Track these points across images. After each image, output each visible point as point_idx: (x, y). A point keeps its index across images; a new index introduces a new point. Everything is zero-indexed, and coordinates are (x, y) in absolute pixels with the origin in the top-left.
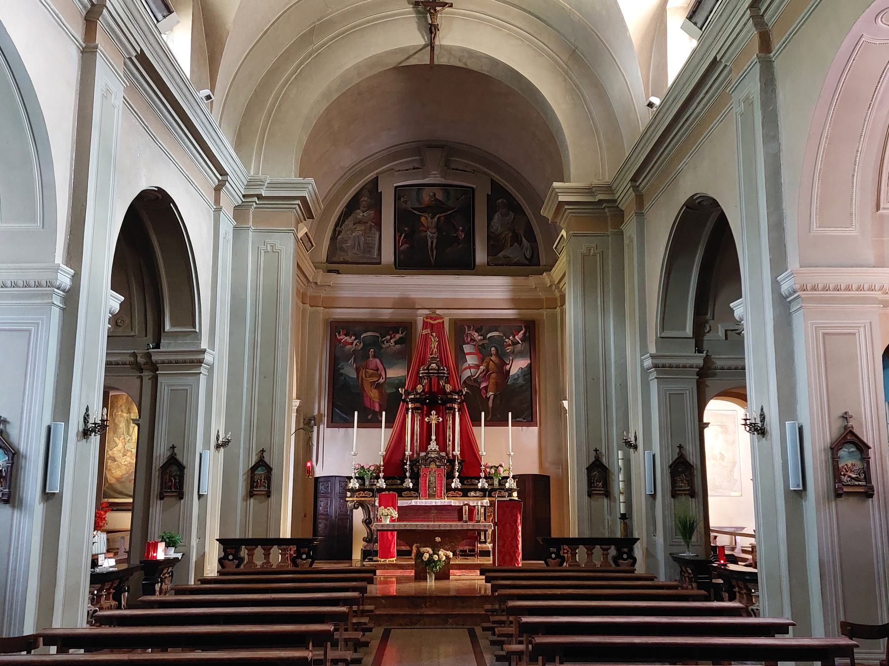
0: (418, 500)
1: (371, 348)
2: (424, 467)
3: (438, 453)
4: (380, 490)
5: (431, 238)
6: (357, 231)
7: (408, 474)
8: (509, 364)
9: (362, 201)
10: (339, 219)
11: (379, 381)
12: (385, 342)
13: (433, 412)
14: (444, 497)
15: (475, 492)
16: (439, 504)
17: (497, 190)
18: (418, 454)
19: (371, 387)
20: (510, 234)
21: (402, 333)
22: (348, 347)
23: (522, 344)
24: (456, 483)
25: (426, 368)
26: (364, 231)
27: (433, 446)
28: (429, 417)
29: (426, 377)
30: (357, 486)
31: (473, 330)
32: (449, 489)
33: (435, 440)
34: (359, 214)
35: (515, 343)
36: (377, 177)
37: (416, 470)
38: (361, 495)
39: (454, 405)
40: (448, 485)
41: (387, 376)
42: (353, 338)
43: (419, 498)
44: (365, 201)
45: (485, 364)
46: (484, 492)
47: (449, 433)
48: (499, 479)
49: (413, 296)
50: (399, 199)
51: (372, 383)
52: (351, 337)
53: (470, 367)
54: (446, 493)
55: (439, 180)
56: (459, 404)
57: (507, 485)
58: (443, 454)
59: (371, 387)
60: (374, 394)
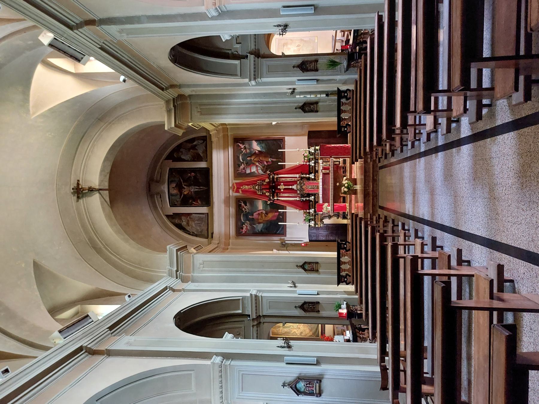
0: (320, 193)
3: (298, 185)
4: (315, 211)
7: (308, 199)
10: (187, 233)
13: (279, 187)
16: (322, 184)
18: (298, 194)
22: (248, 228)
24: (312, 176)
25: (258, 191)
27: (294, 187)
30: (313, 222)
35: (245, 148)
37: (306, 195)
40: (313, 180)
42: (244, 225)
45: (255, 163)
46: (316, 162)
47: (288, 180)
50: (176, 205)
53: (257, 170)
57: (313, 151)
58: (298, 182)
60: (270, 215)
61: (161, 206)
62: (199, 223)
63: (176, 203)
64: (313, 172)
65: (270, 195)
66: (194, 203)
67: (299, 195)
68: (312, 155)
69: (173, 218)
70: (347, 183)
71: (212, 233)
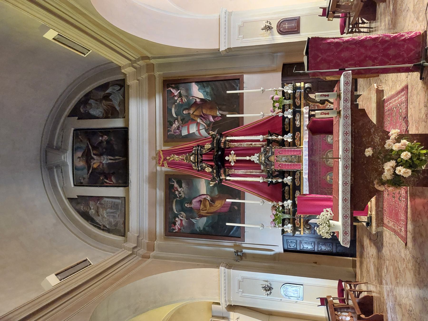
0: (304, 171)
1: (185, 205)
2: (273, 166)
3: (261, 154)
4: (294, 205)
5: (107, 160)
6: (103, 214)
7: (280, 180)
8: (196, 99)
9: (84, 210)
10: (95, 226)
11: (209, 200)
12: (180, 195)
13: (227, 158)
14: (300, 148)
15: (296, 120)
16: (307, 153)
17: (74, 113)
18: (263, 171)
19: (213, 206)
20: (104, 101)
21: (174, 182)
22: (184, 223)
23: (181, 90)
24: (288, 138)
25: (193, 165)
26: (103, 209)
27: (255, 158)
28: (231, 162)
29: (201, 164)
30: (290, 225)
31: (171, 128)
32: (293, 144)
33: (250, 157)
34: (92, 212)
35: (180, 95)
36: (68, 198)
37: (276, 173)
38: (299, 222)
39: (222, 141)
40: (289, 144)
41: (206, 194)
42: (177, 219)
43: (301, 171)
44: (83, 208)
45: (196, 118)
46: (297, 112)
47: (245, 144)
48: (284, 99)
49: (148, 174)
50: (81, 183)
51: (211, 205)
52: (177, 221)
53: (199, 130)
54: (297, 146)
55: (69, 152)
56: (222, 137)
57: (290, 91)
58: (262, 149)
59: (213, 206)
60: (218, 204)
61: (63, 184)
62: (112, 213)
63: (82, 181)
64: (291, 130)
65: (213, 172)
66: (107, 181)
67: (264, 173)
68: (289, 99)
69: (78, 203)
70: (409, 149)
71: (129, 229)
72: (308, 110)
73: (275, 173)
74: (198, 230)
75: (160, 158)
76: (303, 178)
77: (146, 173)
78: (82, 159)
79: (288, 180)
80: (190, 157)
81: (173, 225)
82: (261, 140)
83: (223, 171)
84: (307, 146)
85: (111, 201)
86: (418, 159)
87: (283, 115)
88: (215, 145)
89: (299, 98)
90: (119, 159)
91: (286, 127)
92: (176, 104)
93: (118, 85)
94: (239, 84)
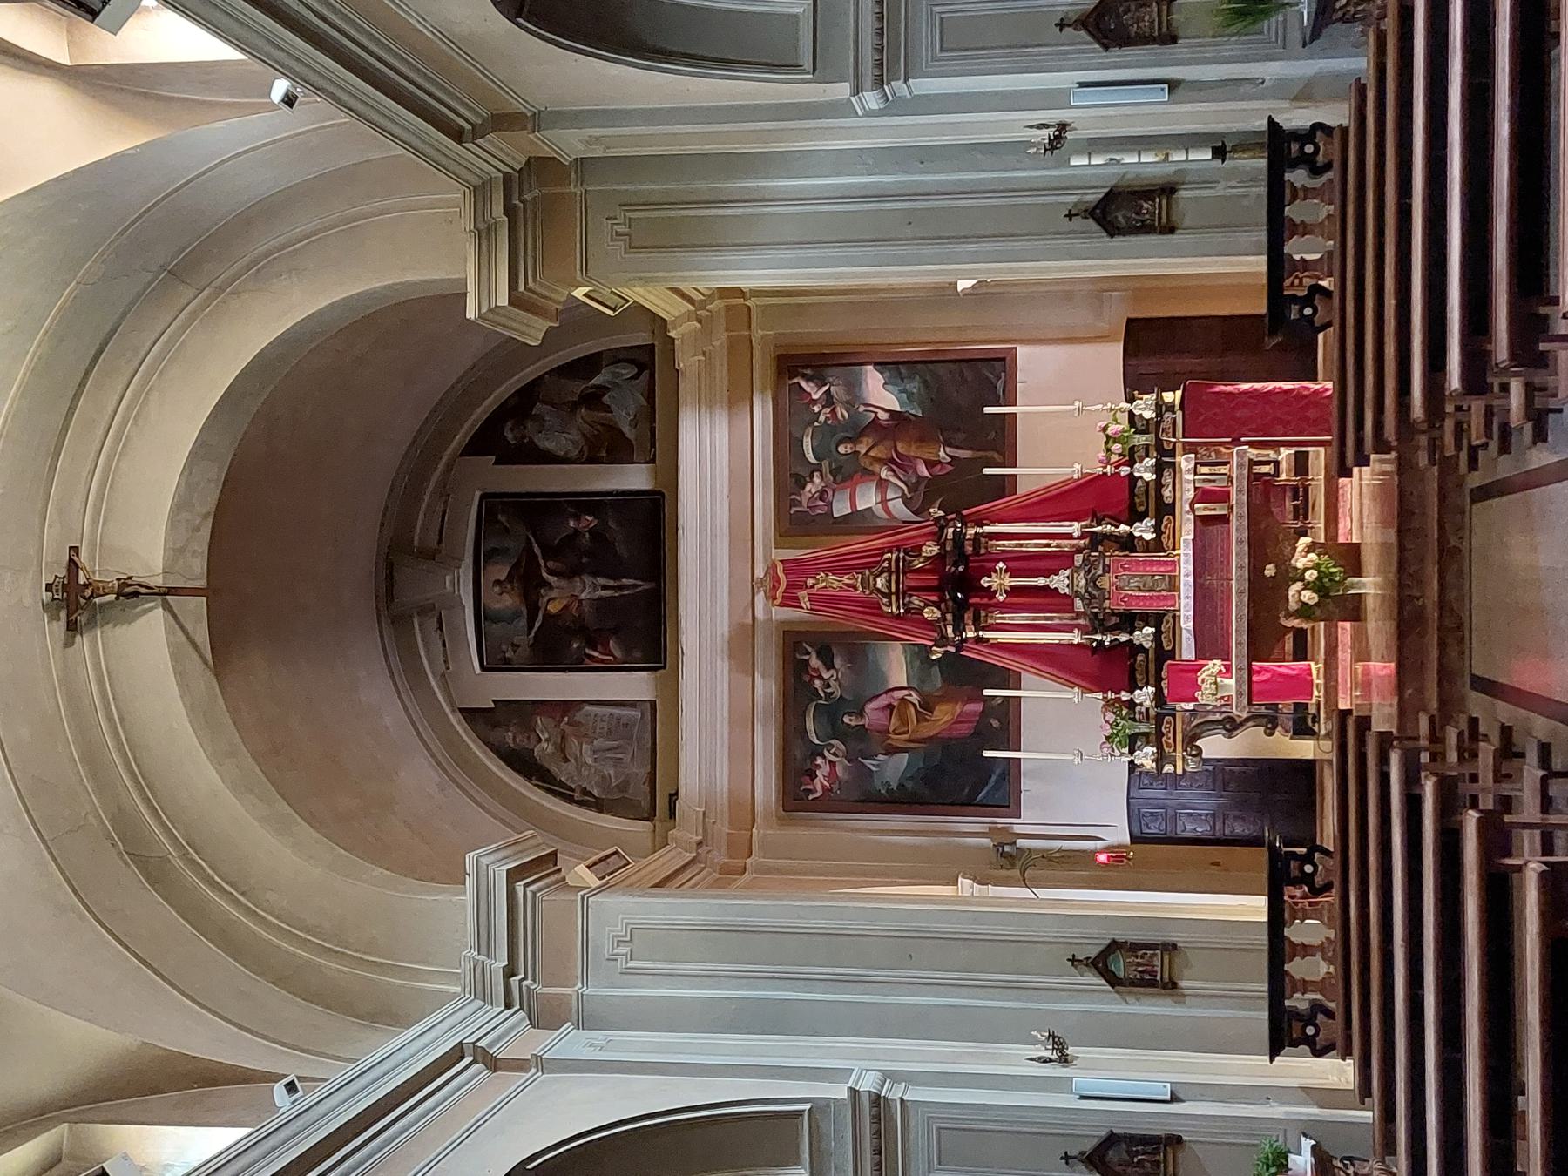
0: (1182, 613)
1: (843, 721)
2: (1107, 602)
4: (1159, 698)
5: (595, 589)
6: (581, 754)
7: (1124, 638)
8: (876, 413)
11: (917, 703)
12: (829, 690)
13: (985, 582)
15: (1163, 486)
16: (1191, 568)
17: (486, 442)
18: (1079, 615)
22: (839, 771)
23: (832, 385)
24: (1144, 530)
25: (885, 600)
27: (1060, 582)
28: (996, 592)
29: (907, 599)
30: (1150, 750)
31: (800, 495)
32: (1157, 546)
35: (829, 400)
36: (461, 710)
37: (1114, 620)
38: (1171, 741)
39: (968, 537)
40: (1148, 547)
41: (905, 685)
42: (819, 761)
43: (1177, 613)
44: (514, 738)
45: (876, 468)
47: (1031, 546)
49: (726, 629)
50: (507, 661)
51: (921, 718)
52: (819, 766)
53: (884, 502)
54: (1165, 551)
57: (1148, 414)
58: (1078, 559)
60: (944, 715)
66: (596, 654)
70: (1317, 567)
72: (1193, 463)
73: (1110, 620)
74: (883, 791)
75: (776, 584)
76: (1181, 629)
77: (723, 628)
78: (509, 586)
79: (1143, 636)
80: (875, 579)
81: (808, 778)
82: (1075, 535)
83: (971, 615)
84: (1191, 552)
85: (593, 715)
86: (1331, 580)
87: (1131, 474)
88: (948, 548)
89: (1171, 430)
90: (635, 586)
91: (1137, 500)
92: (816, 424)
93: (632, 362)
94: (1003, 374)
